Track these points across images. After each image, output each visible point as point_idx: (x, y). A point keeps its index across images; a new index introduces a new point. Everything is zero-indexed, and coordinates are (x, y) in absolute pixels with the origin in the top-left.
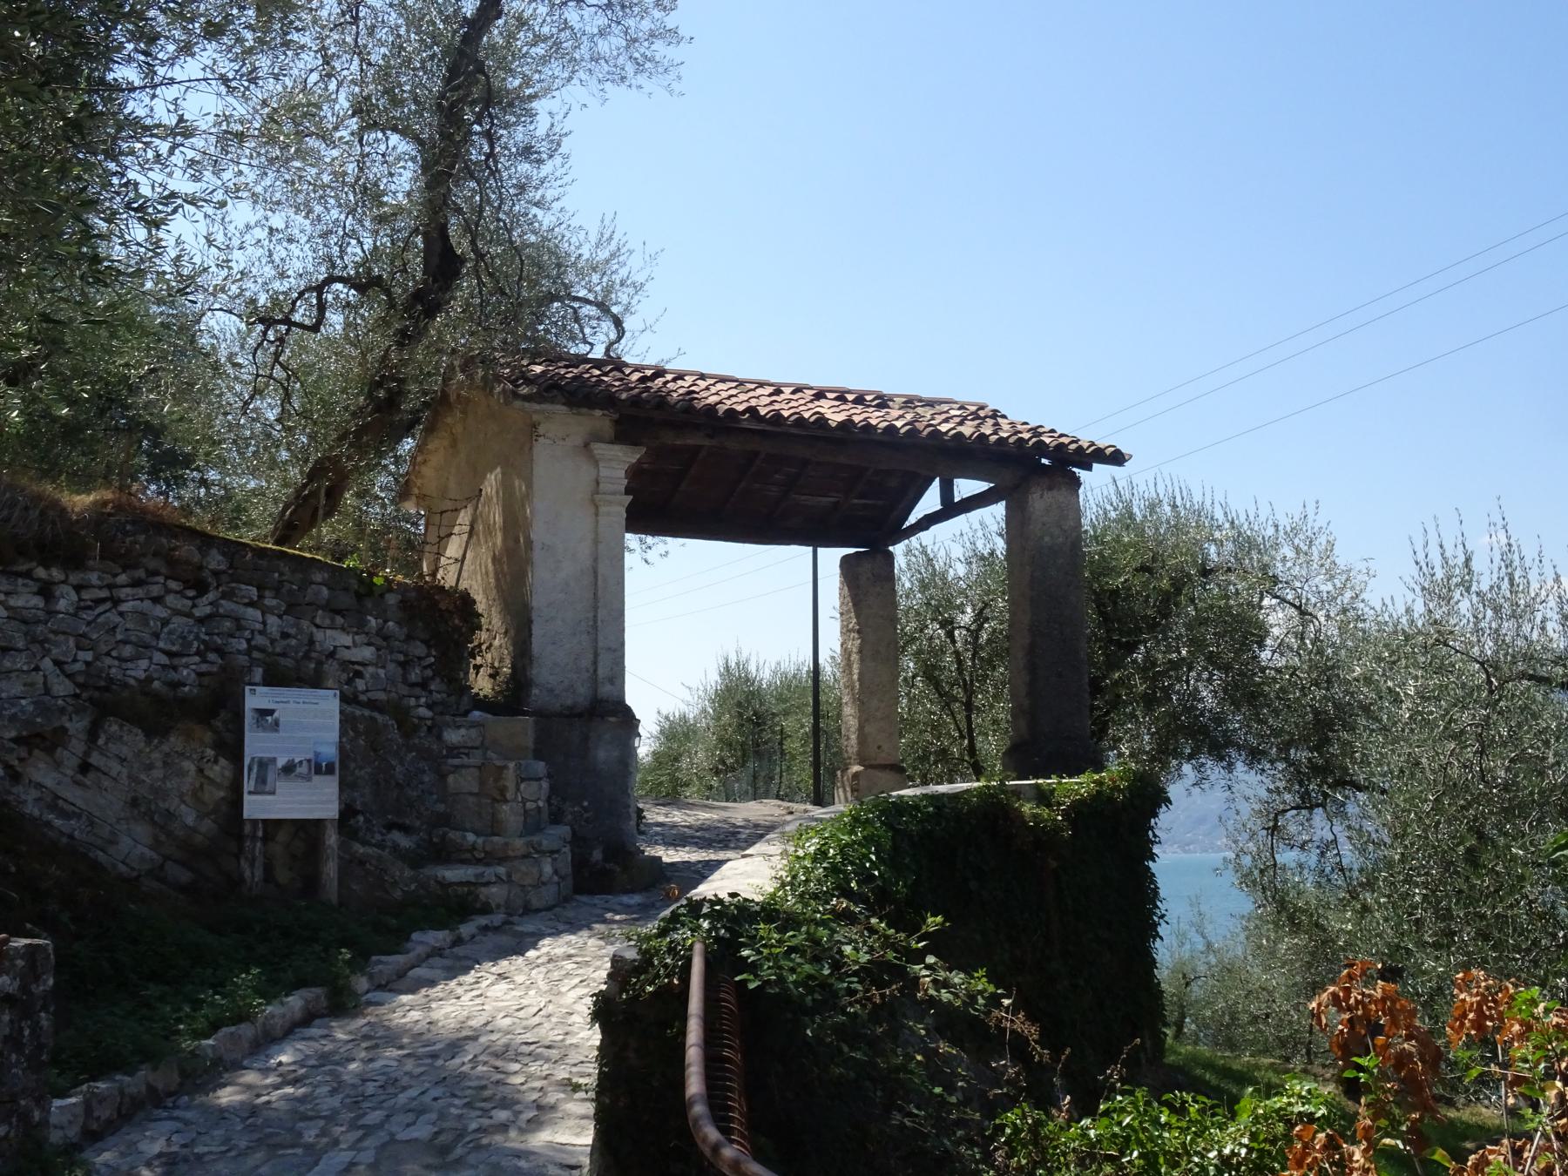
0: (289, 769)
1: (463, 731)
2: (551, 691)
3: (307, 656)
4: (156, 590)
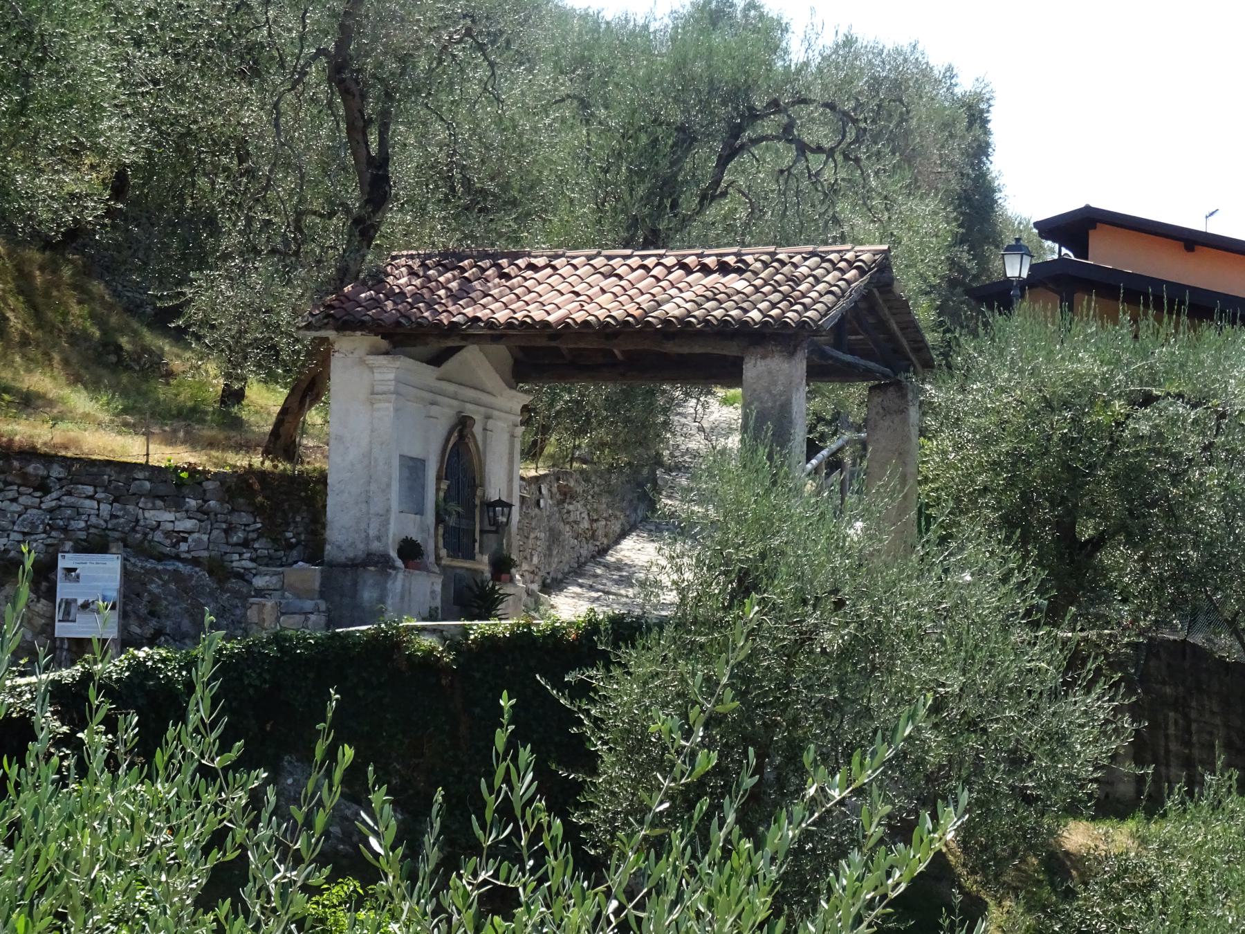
0: (85, 606)
1: (267, 578)
2: (339, 547)
3: (133, 530)
4: (11, 495)
